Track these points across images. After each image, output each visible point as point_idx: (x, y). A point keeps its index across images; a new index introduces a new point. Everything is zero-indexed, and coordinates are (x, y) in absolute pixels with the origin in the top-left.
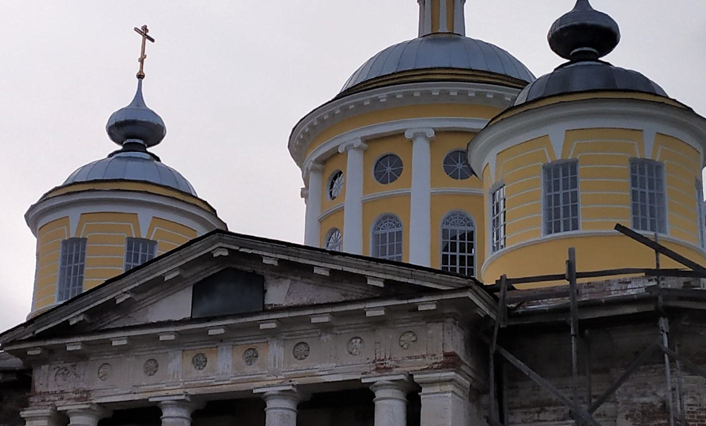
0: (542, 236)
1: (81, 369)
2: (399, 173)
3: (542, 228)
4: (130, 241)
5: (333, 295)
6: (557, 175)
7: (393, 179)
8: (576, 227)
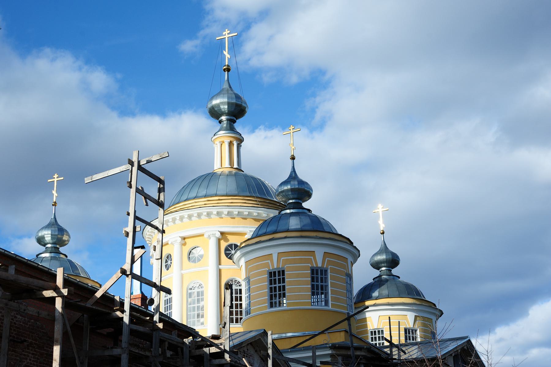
1: (316, 134)
5: (418, 303)
6: (275, 276)
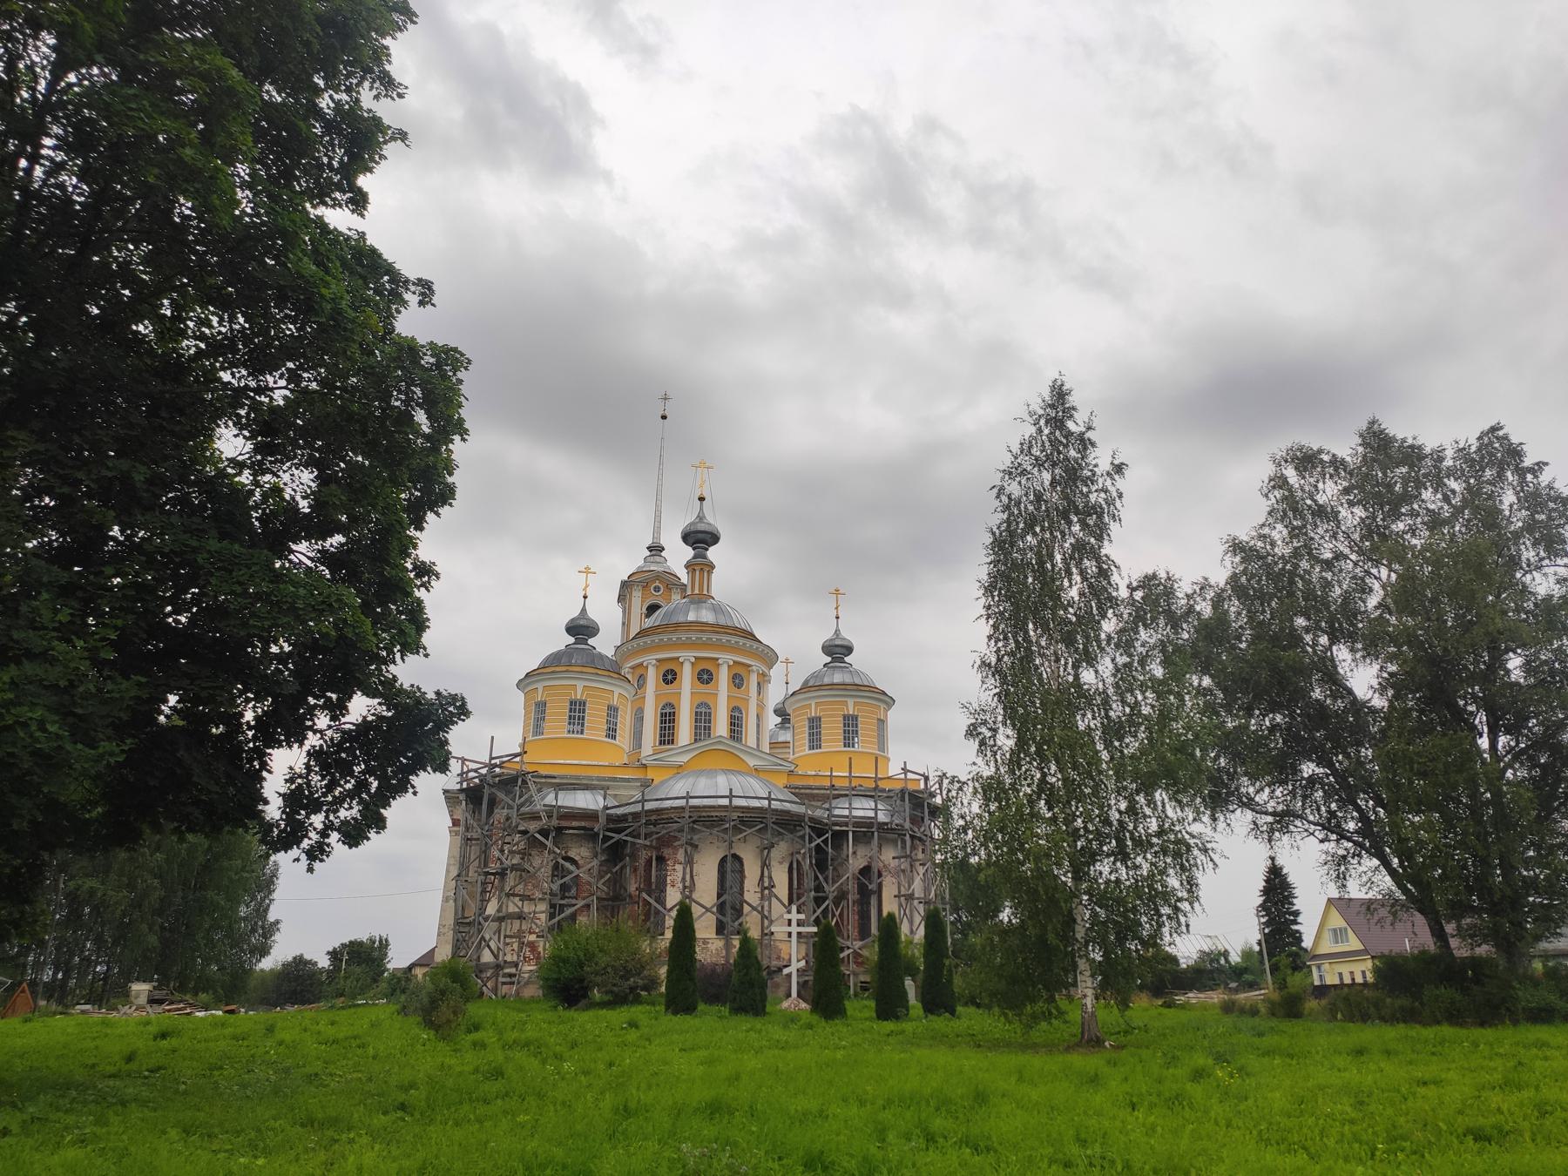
0: (807, 752)
2: (675, 679)
3: (807, 748)
4: (571, 703)
7: (672, 682)
8: (582, 733)
